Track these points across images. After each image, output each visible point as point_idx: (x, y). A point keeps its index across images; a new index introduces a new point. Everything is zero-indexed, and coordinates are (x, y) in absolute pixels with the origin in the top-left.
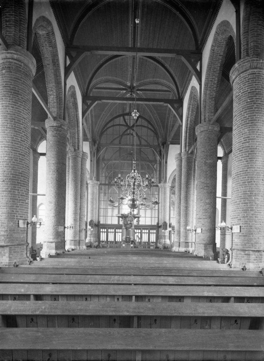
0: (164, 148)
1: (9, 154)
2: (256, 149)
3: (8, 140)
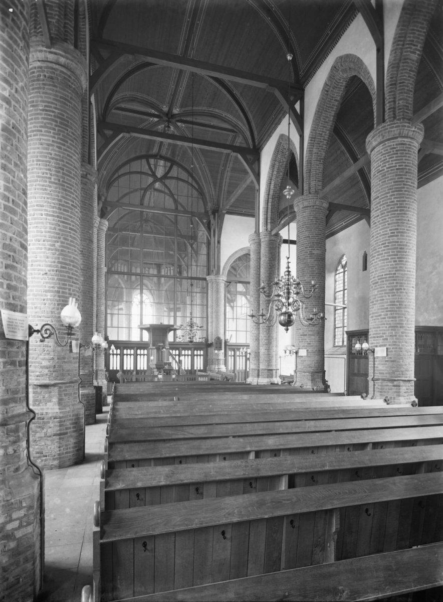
0: (214, 218)
1: (55, 229)
2: (406, 246)
3: (53, 203)
